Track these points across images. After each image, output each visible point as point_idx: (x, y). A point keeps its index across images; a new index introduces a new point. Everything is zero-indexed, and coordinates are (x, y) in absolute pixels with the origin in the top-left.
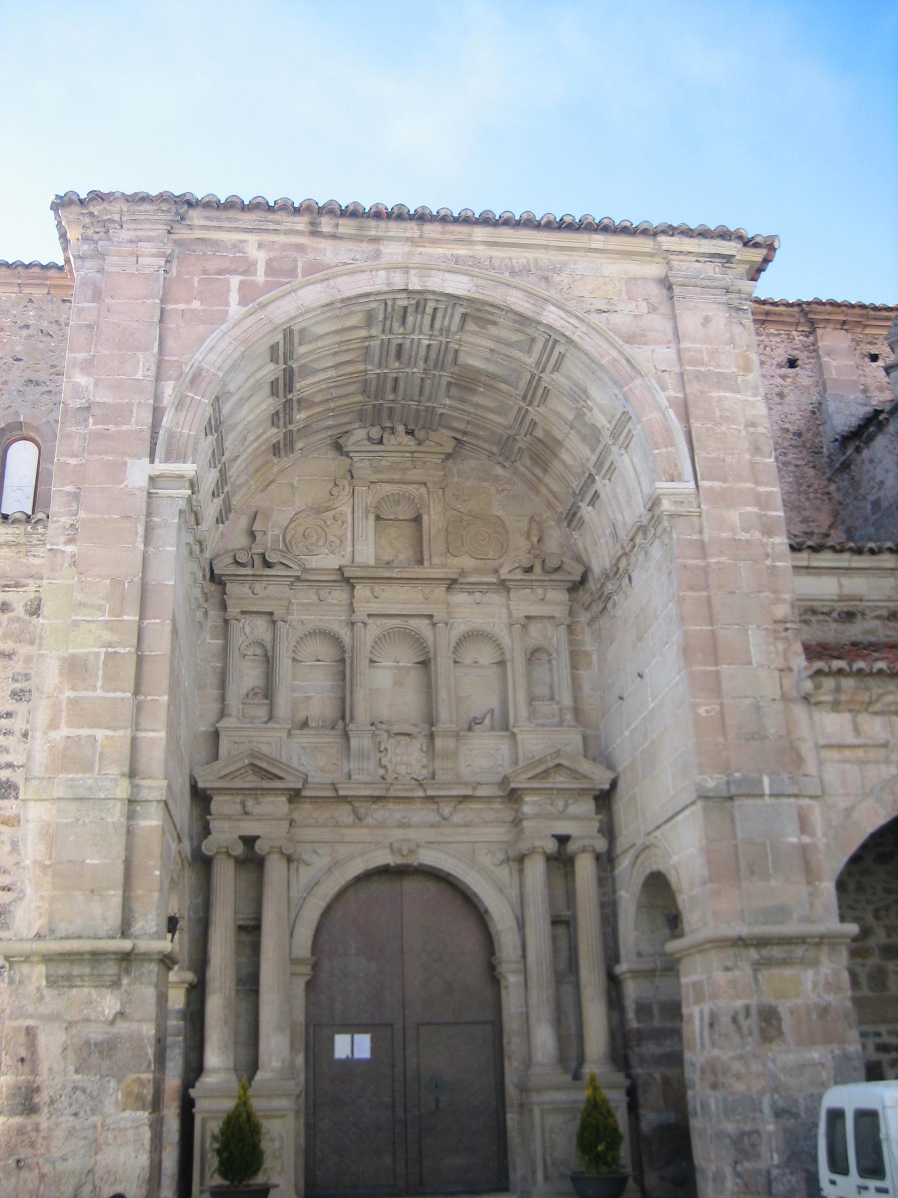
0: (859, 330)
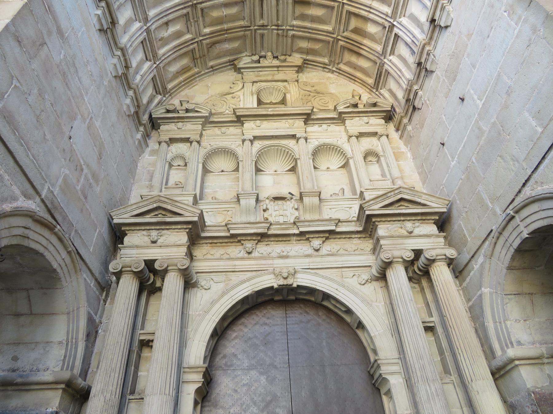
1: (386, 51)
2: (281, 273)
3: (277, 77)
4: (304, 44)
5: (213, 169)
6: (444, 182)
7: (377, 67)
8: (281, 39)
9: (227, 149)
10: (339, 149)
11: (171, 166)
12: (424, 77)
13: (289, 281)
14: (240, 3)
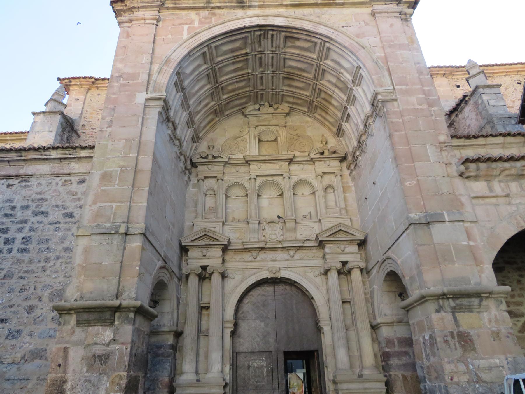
0: (450, 77)
3: (272, 123)
4: (291, 100)
8: (274, 96)
11: (206, 195)
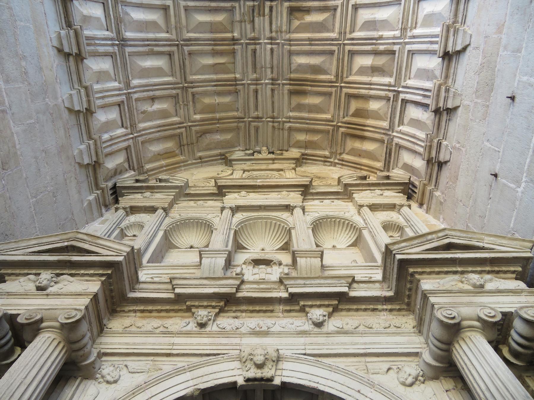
1: (394, 123)
2: (252, 357)
4: (302, 137)
5: (179, 244)
6: (512, 225)
7: (385, 145)
8: (276, 132)
9: (201, 220)
10: (347, 222)
12: (446, 122)
13: (267, 373)
14: (233, 93)
